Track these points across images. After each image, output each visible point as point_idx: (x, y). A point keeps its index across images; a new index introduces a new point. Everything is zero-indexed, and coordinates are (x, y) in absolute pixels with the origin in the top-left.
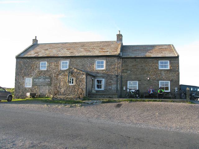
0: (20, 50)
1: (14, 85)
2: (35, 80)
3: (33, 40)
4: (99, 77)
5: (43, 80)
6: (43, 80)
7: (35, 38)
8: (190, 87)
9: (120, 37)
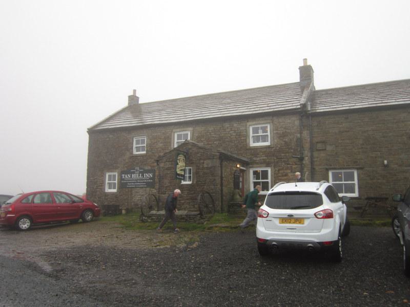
0: (96, 117)
1: (85, 187)
2: (123, 175)
3: (129, 97)
4: (257, 163)
5: (139, 175)
6: (139, 175)
7: (132, 94)
8: (35, 194)
9: (306, 72)
